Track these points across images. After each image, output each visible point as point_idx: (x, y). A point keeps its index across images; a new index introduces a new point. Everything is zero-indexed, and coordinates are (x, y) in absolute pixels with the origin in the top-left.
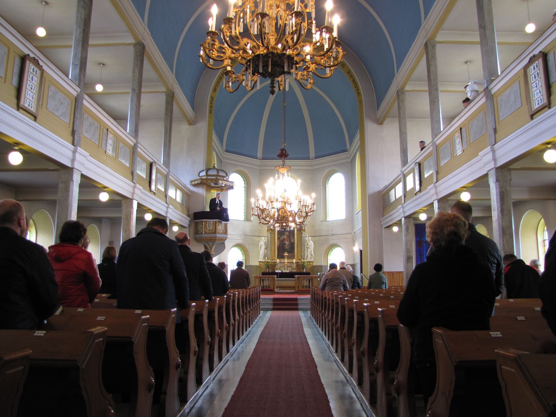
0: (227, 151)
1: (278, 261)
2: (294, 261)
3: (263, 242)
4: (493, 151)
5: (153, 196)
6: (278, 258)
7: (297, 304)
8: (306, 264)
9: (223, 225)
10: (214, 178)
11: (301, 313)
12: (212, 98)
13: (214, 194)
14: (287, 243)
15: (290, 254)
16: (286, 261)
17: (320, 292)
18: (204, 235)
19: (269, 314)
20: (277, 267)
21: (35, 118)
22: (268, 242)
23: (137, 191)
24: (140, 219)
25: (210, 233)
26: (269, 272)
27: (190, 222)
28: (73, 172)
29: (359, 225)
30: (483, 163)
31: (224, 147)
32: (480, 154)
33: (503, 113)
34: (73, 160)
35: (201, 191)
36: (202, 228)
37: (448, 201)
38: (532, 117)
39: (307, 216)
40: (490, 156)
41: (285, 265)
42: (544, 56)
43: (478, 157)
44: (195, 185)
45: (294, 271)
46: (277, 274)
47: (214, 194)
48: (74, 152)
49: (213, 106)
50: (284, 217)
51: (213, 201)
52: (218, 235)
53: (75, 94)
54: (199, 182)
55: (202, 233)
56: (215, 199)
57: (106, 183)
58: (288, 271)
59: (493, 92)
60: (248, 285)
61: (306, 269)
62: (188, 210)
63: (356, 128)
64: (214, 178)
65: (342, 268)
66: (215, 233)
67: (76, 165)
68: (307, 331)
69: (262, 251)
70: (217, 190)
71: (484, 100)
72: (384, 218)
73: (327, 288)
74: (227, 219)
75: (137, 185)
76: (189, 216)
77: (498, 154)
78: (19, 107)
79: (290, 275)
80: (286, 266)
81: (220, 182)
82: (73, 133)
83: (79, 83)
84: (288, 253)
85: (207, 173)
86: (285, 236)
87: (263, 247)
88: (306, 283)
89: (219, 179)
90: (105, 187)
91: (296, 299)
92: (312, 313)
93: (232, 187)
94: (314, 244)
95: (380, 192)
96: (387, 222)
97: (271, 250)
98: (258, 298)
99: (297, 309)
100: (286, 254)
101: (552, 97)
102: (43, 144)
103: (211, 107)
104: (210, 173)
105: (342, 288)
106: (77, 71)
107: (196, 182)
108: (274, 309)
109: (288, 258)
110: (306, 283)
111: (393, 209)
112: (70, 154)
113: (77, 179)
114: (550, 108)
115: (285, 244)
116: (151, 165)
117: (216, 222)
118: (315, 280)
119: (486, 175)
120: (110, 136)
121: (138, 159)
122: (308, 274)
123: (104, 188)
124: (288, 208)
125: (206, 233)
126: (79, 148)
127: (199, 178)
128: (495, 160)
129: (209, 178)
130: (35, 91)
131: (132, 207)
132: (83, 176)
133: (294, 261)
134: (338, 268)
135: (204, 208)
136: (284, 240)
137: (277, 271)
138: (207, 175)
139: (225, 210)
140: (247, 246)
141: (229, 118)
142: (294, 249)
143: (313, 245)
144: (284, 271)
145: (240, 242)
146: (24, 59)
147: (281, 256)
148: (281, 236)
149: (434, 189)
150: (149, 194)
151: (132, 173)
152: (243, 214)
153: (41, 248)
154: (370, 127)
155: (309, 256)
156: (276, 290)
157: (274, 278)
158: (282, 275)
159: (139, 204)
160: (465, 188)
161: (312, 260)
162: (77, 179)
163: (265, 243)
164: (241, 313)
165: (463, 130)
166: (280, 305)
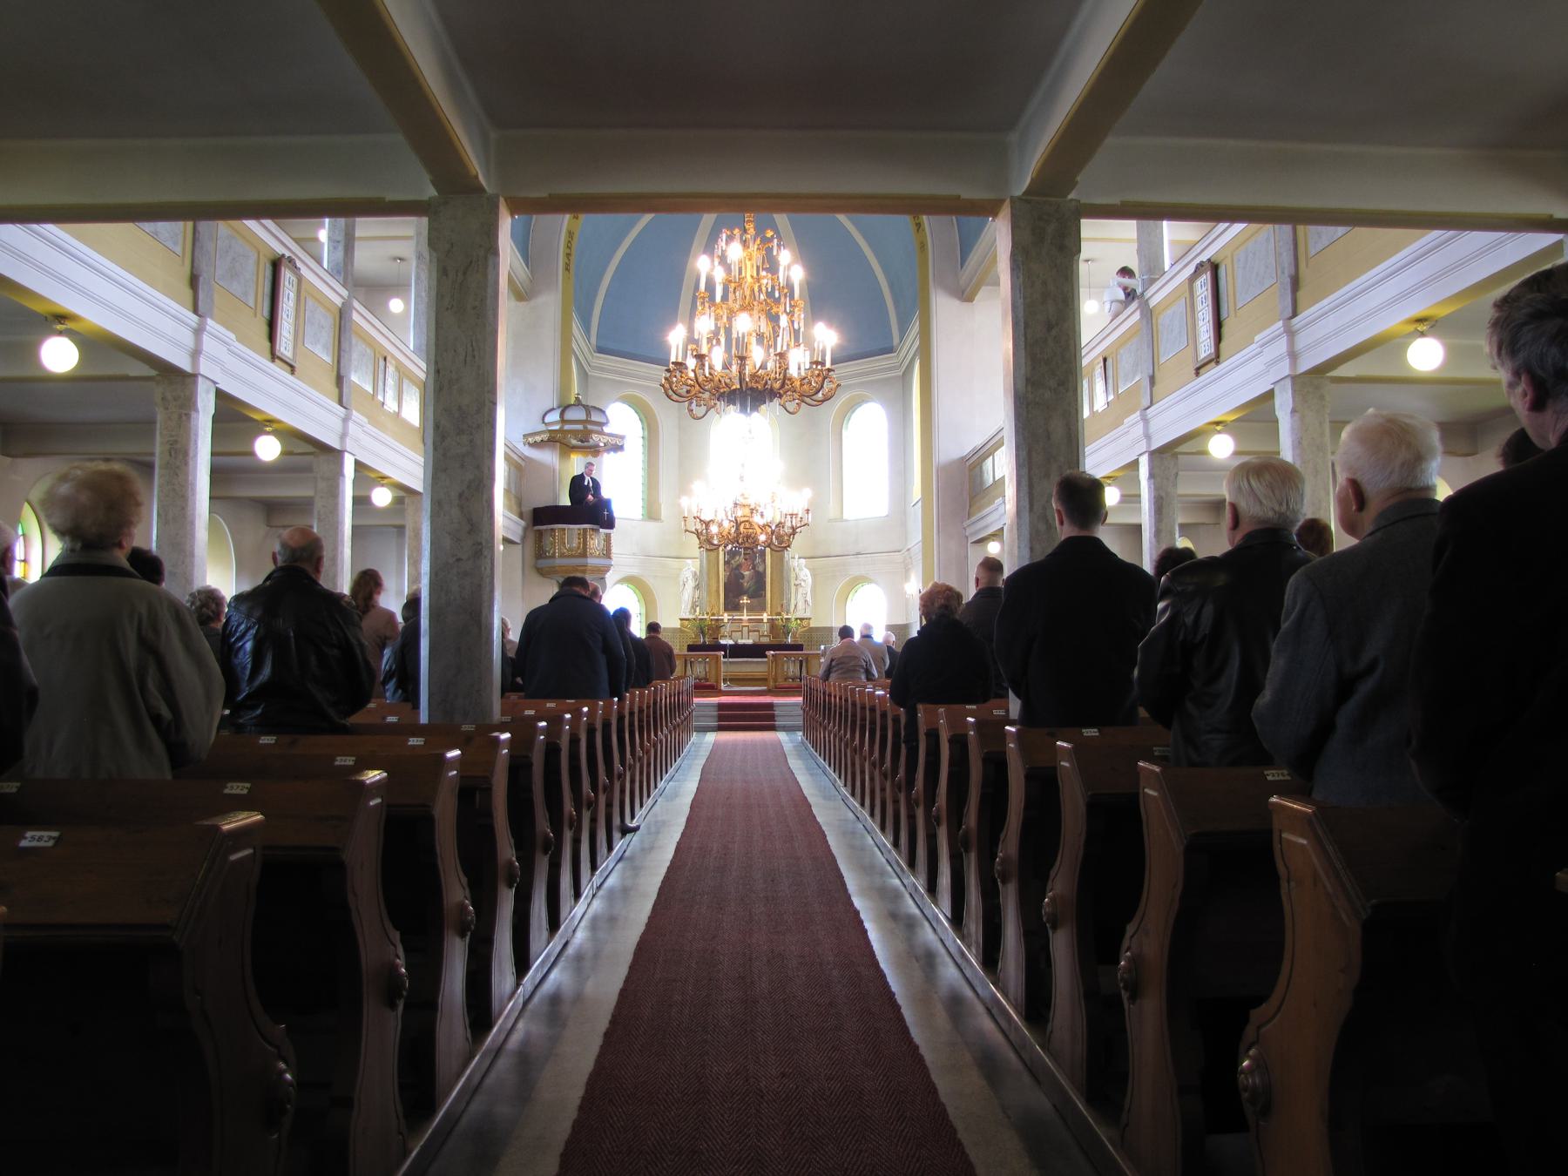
0: (600, 350)
1: (726, 617)
2: (765, 617)
3: (691, 567)
4: (1146, 421)
5: (284, 374)
6: (726, 609)
7: (772, 718)
8: (793, 625)
9: (602, 537)
10: (580, 427)
11: (782, 736)
12: (570, 234)
13: (576, 464)
15: (755, 601)
16: (745, 617)
17: (820, 686)
18: (558, 562)
19: (711, 737)
20: (726, 630)
21: (292, 369)
23: (208, 343)
24: (361, 502)
26: (706, 644)
27: (525, 529)
28: (195, 383)
29: (916, 537)
30: (1255, 368)
31: (594, 340)
32: (1257, 338)
33: (1168, 351)
34: (196, 354)
35: (547, 457)
36: (553, 544)
37: (1175, 455)
38: (1198, 371)
39: (794, 533)
40: (1139, 429)
41: (741, 627)
42: (1215, 268)
43: (1253, 346)
44: (535, 445)
45: (765, 640)
46: (723, 647)
47: (576, 464)
48: (198, 332)
49: (573, 252)
50: (748, 537)
51: (577, 482)
52: (590, 561)
53: (338, 302)
54: (545, 437)
55: (553, 556)
56: (581, 477)
57: (387, 472)
58: (750, 642)
59: (1152, 303)
60: (672, 672)
61: (794, 636)
62: (520, 503)
63: (916, 307)
64: (580, 427)
65: (867, 637)
66: (584, 555)
67: (205, 368)
68: (795, 764)
69: (688, 593)
70: (587, 454)
71: (1137, 316)
72: (973, 519)
73: (833, 676)
74: (610, 524)
75: (209, 321)
76: (521, 516)
77: (1154, 425)
78: (274, 356)
79: (756, 651)
81: (595, 436)
82: (194, 281)
83: (345, 280)
84: (750, 597)
85: (562, 415)
87: (691, 584)
88: (792, 669)
89: (592, 432)
90: (384, 478)
91: (770, 706)
92: (806, 735)
93: (618, 448)
94: (814, 576)
95: (963, 460)
96: (976, 533)
97: (709, 593)
98: (689, 703)
99: (773, 728)
100: (745, 600)
101: (1223, 345)
102: (83, 292)
103: (568, 255)
104: (569, 415)
105: (863, 677)
106: (340, 254)
107: (538, 439)
108: (721, 728)
109: (751, 609)
110: (792, 669)
111: (991, 502)
112: (188, 339)
113: (206, 407)
114: (1218, 363)
115: (743, 577)
116: (276, 264)
118: (814, 662)
119: (1269, 396)
120: (391, 369)
121: (310, 302)
122: (799, 647)
123: (58, 321)
124: (757, 519)
125: (562, 556)
126: (209, 321)
127: (542, 427)
128: (1148, 437)
129: (567, 427)
130: (291, 320)
131: (340, 473)
132: (221, 395)
133: (765, 617)
134: (857, 637)
135: (556, 497)
136: (739, 566)
137: (723, 642)
138: (563, 421)
139: (606, 504)
140: (651, 582)
141: (610, 257)
143: (810, 580)
144: (740, 642)
145: (634, 571)
146: (276, 264)
147: (732, 605)
149: (1284, 339)
150: (266, 363)
151: (340, 380)
152: (640, 503)
153: (10, 571)
154: (943, 307)
155: (801, 605)
156: (723, 687)
157: (717, 657)
158: (737, 651)
159: (358, 464)
160: (1425, 324)
161: (808, 615)
162: (206, 407)
164: (628, 755)
165: (1109, 362)
166: (730, 718)
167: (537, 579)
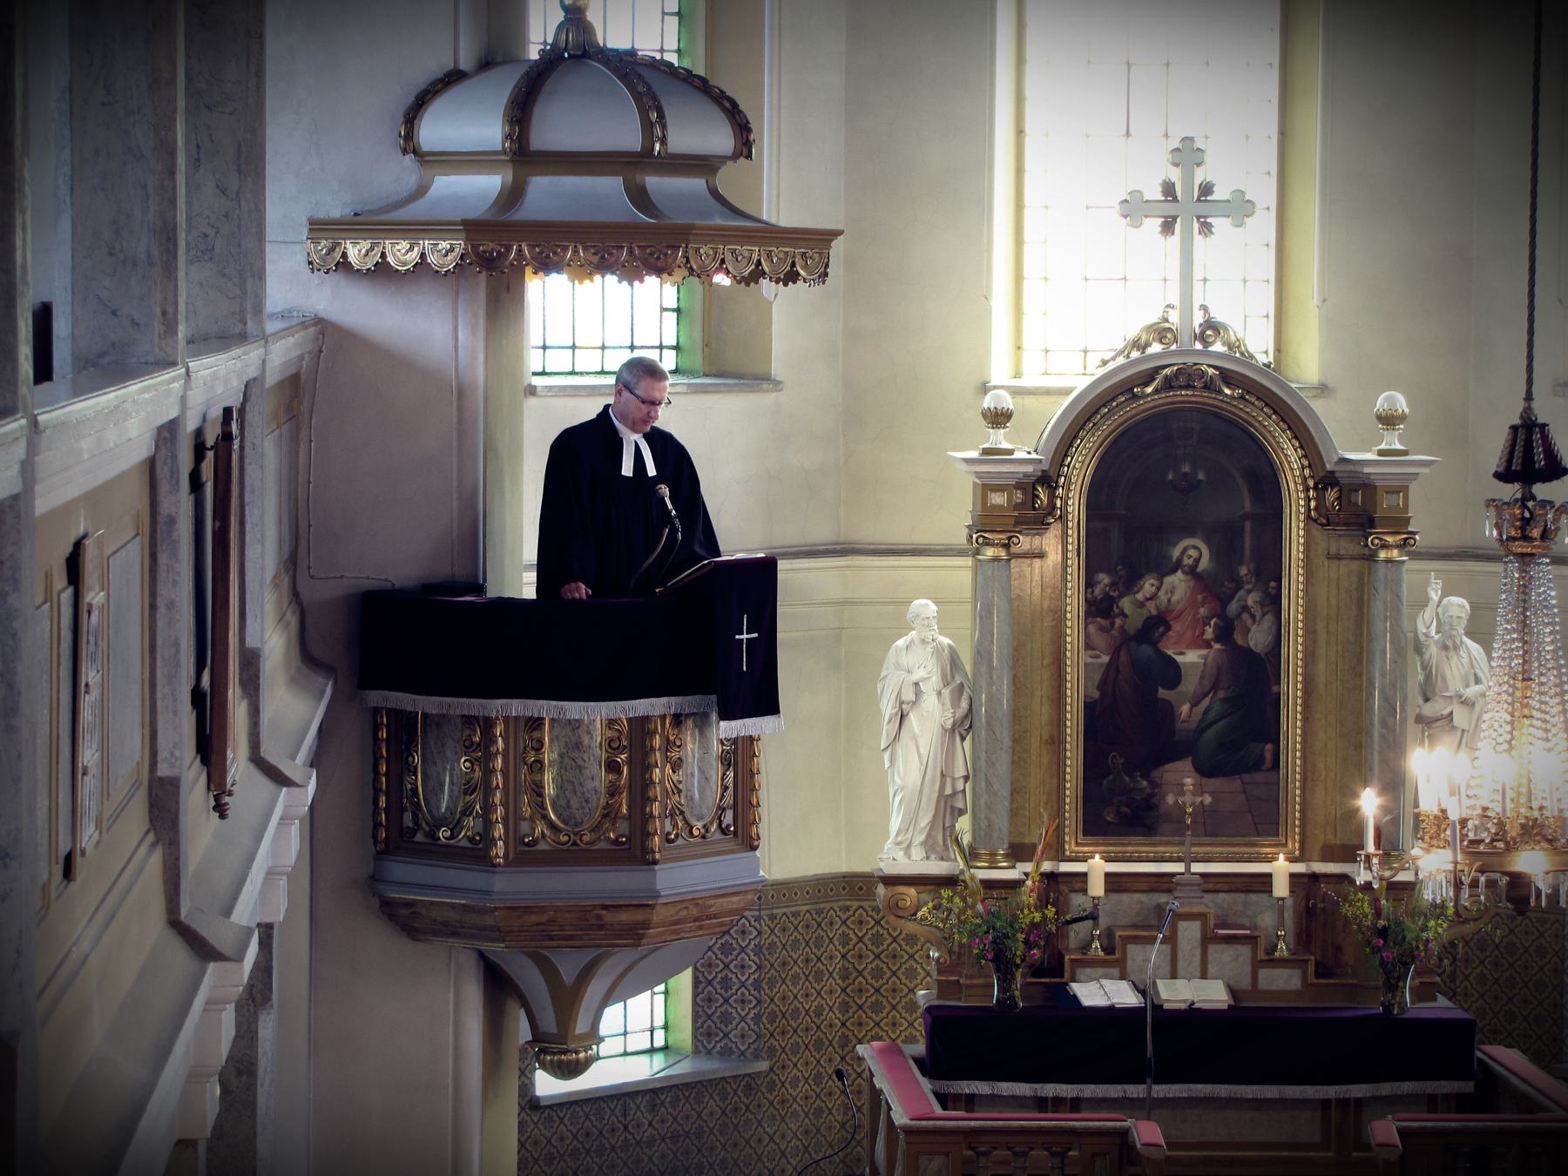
2: (1281, 868)
14: (1190, 658)
22: (981, 654)
25: (570, 855)
55: (477, 853)
58: (1212, 994)
66: (636, 851)
74: (759, 696)
80: (1190, 932)
84: (1204, 771)
85: (520, 112)
86: (1178, 583)
87: (933, 714)
104: (566, 124)
115: (1172, 673)
117: (641, 726)
125: (526, 855)
136: (1157, 624)
138: (523, 155)
142: (1271, 731)
144: (1177, 993)
148: (1130, 582)
163: (954, 661)
167: (378, 942)
